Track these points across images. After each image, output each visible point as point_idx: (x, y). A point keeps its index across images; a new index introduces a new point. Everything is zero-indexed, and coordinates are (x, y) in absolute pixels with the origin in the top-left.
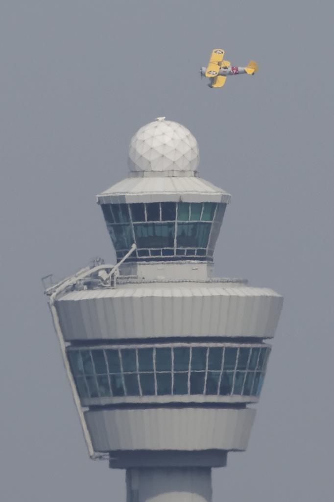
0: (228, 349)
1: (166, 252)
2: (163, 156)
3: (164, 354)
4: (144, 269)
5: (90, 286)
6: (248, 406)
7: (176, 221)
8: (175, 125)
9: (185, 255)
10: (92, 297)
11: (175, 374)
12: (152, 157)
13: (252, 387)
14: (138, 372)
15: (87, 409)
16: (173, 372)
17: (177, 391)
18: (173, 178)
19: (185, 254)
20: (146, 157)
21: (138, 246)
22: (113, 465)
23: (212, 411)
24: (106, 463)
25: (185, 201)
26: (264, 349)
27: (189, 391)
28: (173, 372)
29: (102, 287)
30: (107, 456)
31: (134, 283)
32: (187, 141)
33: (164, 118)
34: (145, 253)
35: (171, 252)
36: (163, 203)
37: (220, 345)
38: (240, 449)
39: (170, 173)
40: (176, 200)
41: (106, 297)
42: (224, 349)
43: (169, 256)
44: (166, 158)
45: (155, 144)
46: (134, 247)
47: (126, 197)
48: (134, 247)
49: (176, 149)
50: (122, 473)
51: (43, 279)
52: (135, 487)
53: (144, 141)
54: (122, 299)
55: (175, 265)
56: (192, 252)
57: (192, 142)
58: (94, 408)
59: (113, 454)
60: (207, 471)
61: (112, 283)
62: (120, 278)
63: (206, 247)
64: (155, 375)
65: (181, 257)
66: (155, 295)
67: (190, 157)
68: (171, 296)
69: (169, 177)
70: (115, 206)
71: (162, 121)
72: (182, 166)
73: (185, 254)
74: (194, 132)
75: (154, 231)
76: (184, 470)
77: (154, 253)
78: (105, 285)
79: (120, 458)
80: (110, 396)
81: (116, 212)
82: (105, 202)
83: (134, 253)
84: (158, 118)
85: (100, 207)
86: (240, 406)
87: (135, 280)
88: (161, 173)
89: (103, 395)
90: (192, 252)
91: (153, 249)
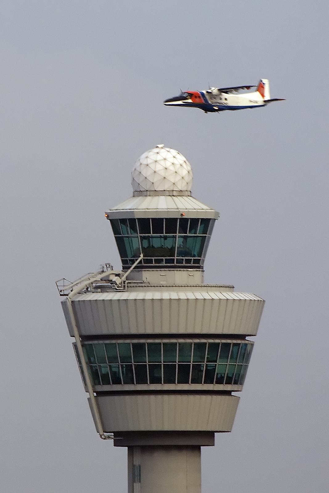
0: (224, 344)
1: (167, 261)
2: (165, 178)
3: (154, 348)
4: (148, 275)
5: (103, 289)
6: (233, 393)
7: (178, 234)
8: (174, 152)
10: (101, 298)
12: (156, 179)
13: (237, 379)
15: (95, 394)
17: (194, 381)
18: (174, 197)
20: (151, 179)
24: (112, 441)
32: (184, 165)
33: (163, 145)
34: (150, 261)
36: (153, 219)
37: (217, 341)
39: (171, 194)
43: (171, 265)
45: (159, 168)
46: (142, 255)
47: (135, 213)
48: (142, 255)
49: (176, 172)
50: (124, 450)
52: (137, 462)
53: (147, 165)
55: (176, 271)
56: (188, 261)
57: (187, 167)
58: (100, 394)
59: (117, 434)
60: (197, 449)
63: (144, 263)
64: (162, 366)
65: (179, 266)
66: (146, 298)
68: (168, 298)
69: (170, 196)
70: (123, 221)
71: (162, 148)
72: (181, 186)
74: (189, 158)
76: (180, 448)
77: (157, 261)
79: (122, 438)
84: (158, 146)
86: (228, 393)
87: (143, 285)
88: (163, 193)
90: (188, 261)
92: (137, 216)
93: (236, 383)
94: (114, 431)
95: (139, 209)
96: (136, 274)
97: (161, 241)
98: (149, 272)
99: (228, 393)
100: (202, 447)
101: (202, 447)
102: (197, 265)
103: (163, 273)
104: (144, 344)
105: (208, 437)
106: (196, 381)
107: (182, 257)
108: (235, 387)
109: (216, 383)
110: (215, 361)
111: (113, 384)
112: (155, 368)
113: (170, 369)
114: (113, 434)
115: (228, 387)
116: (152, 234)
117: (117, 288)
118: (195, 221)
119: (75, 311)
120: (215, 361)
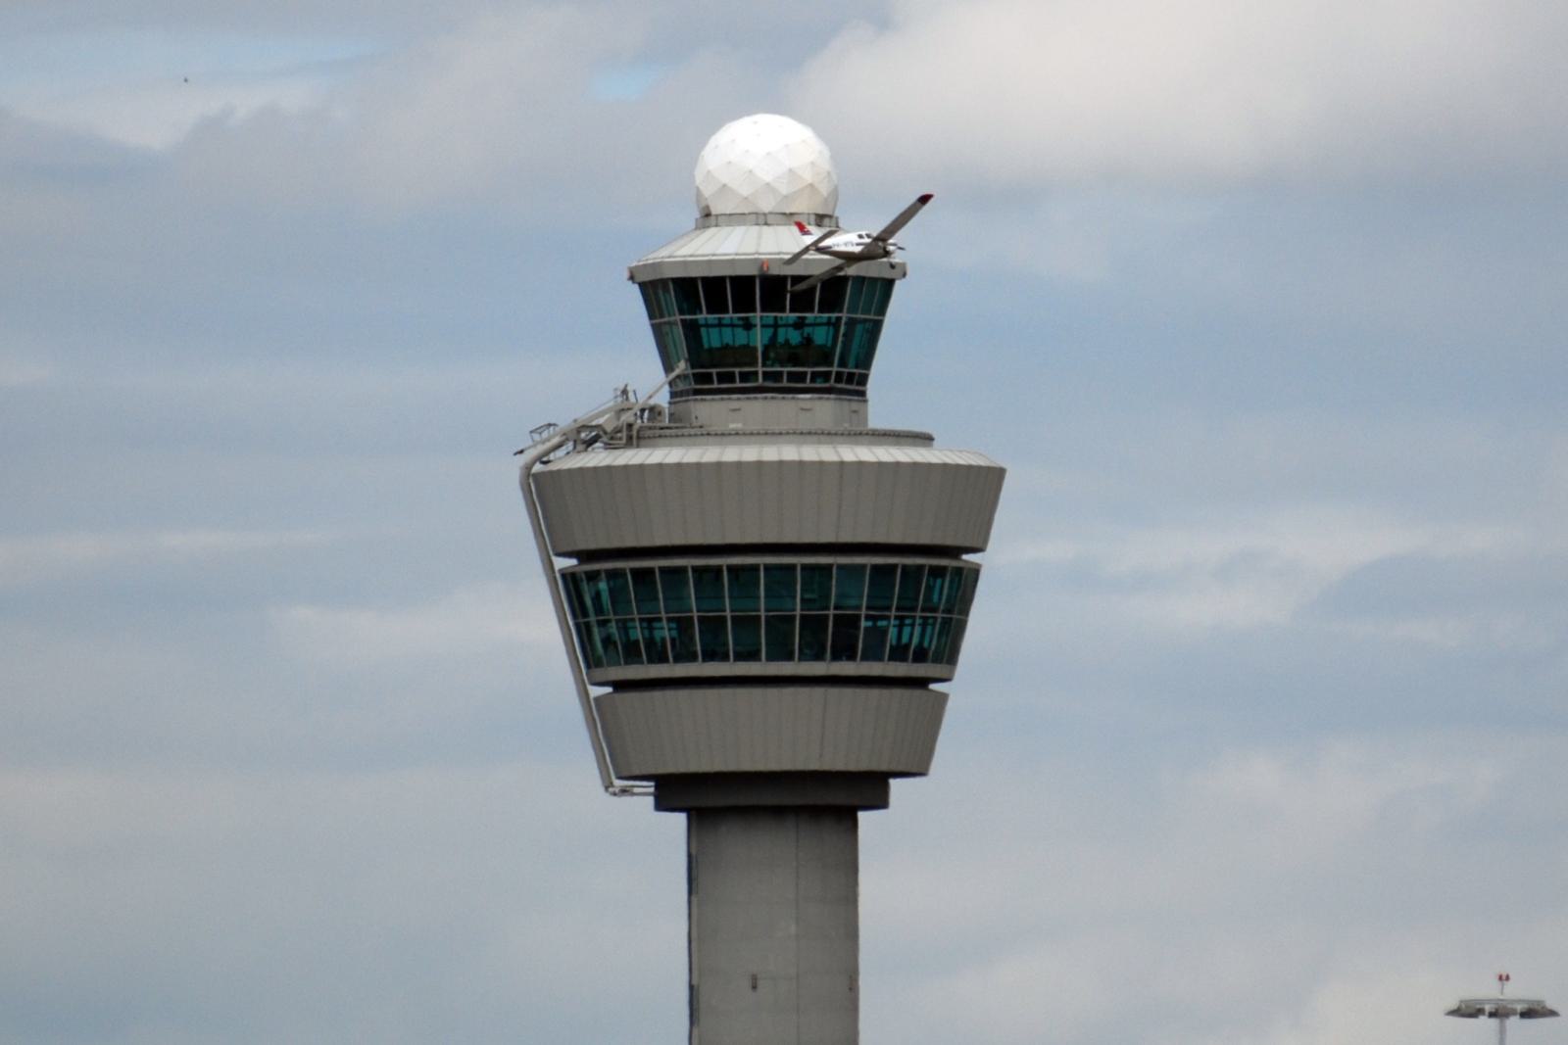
3: (708, 577)
4: (710, 410)
10: (578, 465)
13: (942, 643)
17: (710, 655)
19: (808, 380)
22: (662, 805)
23: (874, 694)
24: (650, 800)
25: (775, 271)
26: (959, 571)
30: (649, 787)
31: (666, 436)
38: (914, 770)
40: (753, 271)
41: (631, 463)
42: (927, 568)
43: (750, 388)
50: (680, 820)
51: (531, 432)
56: (730, 378)
60: (846, 817)
61: (630, 438)
62: (650, 428)
73: (808, 380)
76: (778, 812)
77: (722, 378)
78: (611, 442)
79: (671, 791)
80: (642, 663)
85: (635, 290)
89: (609, 664)
91: (718, 370)
94: (653, 771)
95: (697, 256)
97: (776, 327)
98: (774, 401)
99: (922, 683)
100: (895, 784)
102: (851, 383)
103: (735, 405)
104: (792, 568)
105: (872, 789)
106: (781, 652)
107: (782, 366)
109: (891, 659)
110: (886, 604)
111: (704, 660)
112: (746, 623)
113: (713, 626)
114: (652, 784)
117: (611, 442)
119: (547, 494)
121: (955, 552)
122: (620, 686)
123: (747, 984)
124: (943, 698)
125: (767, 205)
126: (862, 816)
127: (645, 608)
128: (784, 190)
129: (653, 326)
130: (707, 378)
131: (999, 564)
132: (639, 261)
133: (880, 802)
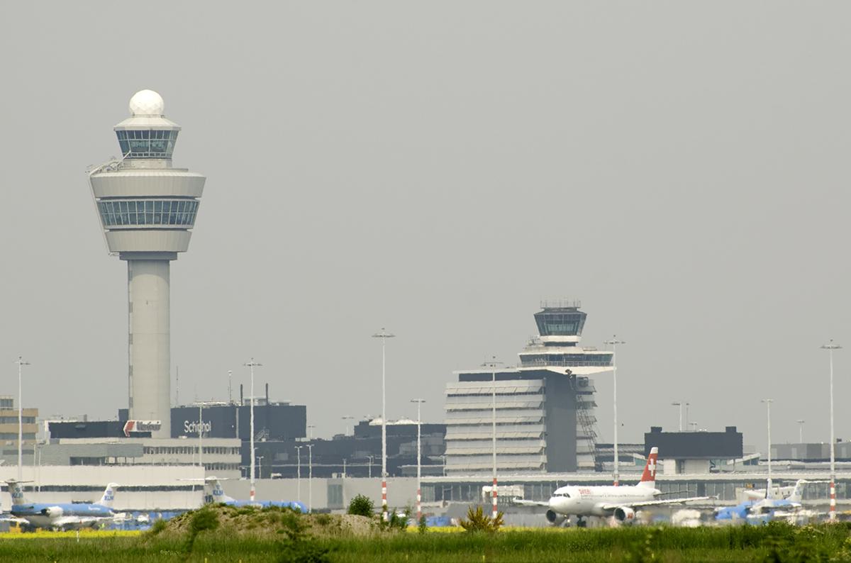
4: (135, 163)
9: (143, 156)
11: (417, 464)
13: (190, 221)
14: (345, 466)
16: (419, 466)
17: (132, 223)
21: (132, 151)
25: (154, 129)
27: (414, 466)
28: (419, 466)
29: (112, 171)
35: (147, 155)
37: (177, 200)
40: (149, 129)
44: (146, 108)
54: (120, 177)
59: (121, 253)
60: (167, 262)
67: (159, 106)
70: (121, 132)
75: (142, 144)
77: (139, 155)
79: (124, 255)
81: (121, 134)
82: (118, 130)
83: (130, 154)
86: (185, 230)
92: (126, 129)
93: (189, 224)
96: (127, 162)
97: (563, 319)
99: (185, 230)
101: (447, 428)
105: (173, 255)
108: (189, 226)
110: (177, 211)
113: (149, 216)
115: (184, 226)
116: (142, 139)
118: (160, 132)
120: (177, 211)
121: (193, 198)
122: (111, 230)
123: (145, 302)
124: (191, 233)
125: (149, 113)
126: (171, 262)
127: (118, 211)
128: (154, 109)
129: (121, 143)
130: (136, 155)
131: (204, 202)
132: (70, 419)
133: (175, 258)
